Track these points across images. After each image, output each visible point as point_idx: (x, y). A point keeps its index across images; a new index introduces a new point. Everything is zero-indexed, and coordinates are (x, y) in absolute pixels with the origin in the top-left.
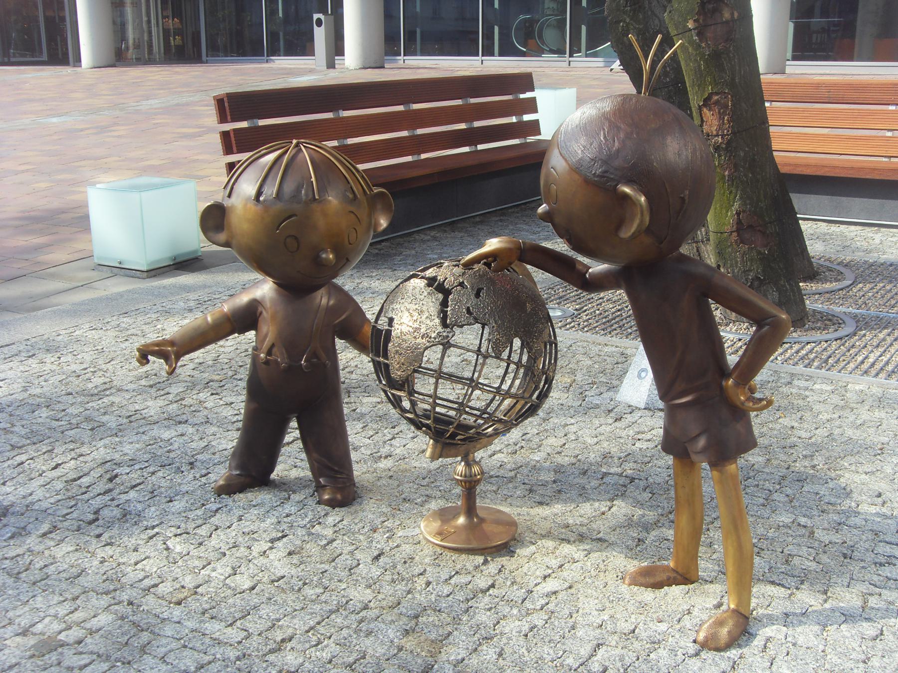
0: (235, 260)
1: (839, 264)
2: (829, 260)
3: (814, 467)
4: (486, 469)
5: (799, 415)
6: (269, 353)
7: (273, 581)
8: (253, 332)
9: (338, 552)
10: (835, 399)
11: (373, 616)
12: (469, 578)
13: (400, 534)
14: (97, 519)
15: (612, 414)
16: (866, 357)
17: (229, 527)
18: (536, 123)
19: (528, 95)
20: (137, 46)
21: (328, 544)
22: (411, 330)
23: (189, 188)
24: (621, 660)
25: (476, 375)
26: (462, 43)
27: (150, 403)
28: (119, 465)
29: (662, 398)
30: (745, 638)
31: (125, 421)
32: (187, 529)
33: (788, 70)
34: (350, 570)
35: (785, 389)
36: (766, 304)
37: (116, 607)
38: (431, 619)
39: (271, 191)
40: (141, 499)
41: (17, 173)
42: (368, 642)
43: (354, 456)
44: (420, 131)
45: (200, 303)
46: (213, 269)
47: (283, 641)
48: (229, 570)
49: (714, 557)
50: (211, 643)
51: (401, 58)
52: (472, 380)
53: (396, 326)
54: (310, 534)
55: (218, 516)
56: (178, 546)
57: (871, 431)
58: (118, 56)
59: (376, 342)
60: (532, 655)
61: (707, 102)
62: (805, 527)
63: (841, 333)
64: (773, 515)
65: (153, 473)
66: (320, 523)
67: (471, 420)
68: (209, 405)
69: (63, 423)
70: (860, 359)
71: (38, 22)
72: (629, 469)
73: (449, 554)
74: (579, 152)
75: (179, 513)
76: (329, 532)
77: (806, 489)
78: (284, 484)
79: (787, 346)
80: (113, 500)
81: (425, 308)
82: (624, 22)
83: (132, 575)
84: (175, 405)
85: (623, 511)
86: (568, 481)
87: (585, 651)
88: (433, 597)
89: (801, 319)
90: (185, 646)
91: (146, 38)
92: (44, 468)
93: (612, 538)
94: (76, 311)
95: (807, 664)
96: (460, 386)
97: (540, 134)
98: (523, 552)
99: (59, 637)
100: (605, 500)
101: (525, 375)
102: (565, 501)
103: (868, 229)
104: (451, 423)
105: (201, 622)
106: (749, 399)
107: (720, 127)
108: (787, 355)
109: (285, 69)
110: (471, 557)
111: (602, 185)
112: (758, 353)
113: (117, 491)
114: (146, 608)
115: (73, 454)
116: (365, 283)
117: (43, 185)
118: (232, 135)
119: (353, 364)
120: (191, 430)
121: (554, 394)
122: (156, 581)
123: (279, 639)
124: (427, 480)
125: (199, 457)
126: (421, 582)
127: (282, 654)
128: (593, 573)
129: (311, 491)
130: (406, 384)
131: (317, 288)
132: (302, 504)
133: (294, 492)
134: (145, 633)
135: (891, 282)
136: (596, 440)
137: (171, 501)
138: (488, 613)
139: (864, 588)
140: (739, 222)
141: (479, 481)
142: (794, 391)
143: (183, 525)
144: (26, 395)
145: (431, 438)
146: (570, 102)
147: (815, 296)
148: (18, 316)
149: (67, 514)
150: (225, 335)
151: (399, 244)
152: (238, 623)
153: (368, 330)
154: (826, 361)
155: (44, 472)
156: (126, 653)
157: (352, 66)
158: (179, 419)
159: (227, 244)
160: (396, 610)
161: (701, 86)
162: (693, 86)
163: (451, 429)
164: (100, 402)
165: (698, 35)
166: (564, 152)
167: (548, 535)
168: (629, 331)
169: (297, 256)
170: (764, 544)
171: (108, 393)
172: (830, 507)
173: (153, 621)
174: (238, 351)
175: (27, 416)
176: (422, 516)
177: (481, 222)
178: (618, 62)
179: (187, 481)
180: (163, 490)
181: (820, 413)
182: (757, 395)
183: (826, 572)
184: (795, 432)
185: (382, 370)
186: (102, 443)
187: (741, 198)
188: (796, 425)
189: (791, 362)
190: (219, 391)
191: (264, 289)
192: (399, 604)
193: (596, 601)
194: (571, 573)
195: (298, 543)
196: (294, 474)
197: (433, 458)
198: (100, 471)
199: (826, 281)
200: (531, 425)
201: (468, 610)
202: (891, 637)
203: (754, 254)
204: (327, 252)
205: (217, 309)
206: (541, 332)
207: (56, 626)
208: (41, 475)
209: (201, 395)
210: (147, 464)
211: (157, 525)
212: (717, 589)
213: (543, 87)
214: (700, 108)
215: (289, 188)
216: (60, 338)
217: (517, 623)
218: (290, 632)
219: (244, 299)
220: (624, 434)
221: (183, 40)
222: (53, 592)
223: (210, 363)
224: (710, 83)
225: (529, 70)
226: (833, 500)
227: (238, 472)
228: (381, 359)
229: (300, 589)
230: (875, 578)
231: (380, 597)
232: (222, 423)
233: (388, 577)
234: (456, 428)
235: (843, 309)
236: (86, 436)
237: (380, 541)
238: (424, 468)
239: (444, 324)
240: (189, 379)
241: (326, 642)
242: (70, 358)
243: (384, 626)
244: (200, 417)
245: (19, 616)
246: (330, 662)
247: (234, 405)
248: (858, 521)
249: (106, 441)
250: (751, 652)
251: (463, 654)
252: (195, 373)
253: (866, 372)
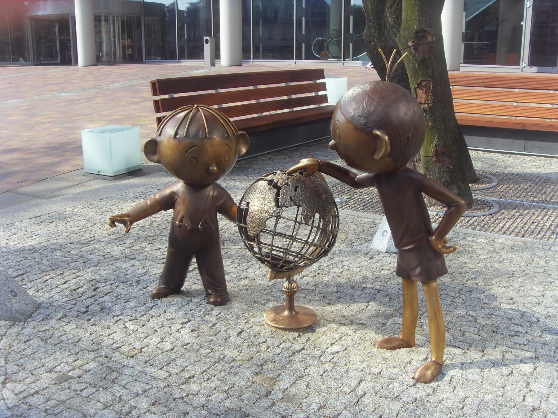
0: (160, 170)
1: (490, 174)
2: (484, 172)
3: (477, 284)
4: (299, 285)
5: (469, 256)
6: (181, 221)
7: (183, 346)
8: (172, 210)
9: (219, 330)
10: (488, 247)
11: (238, 365)
12: (290, 344)
13: (252, 320)
14: (88, 311)
15: (368, 255)
16: (505, 225)
17: (159, 316)
18: (325, 96)
19: (321, 81)
20: (108, 55)
21: (213, 326)
22: (259, 209)
23: (136, 131)
24: (373, 389)
25: (295, 233)
26: (284, 52)
27: (115, 248)
28: (98, 282)
29: (396, 246)
30: (440, 376)
31: (102, 258)
33: (461, 69)
34: (225, 340)
35: (461, 242)
36: (452, 195)
37: (99, 359)
38: (270, 367)
39: (182, 132)
41: (43, 123)
42: (236, 379)
43: (227, 278)
44: (262, 100)
45: (142, 194)
46: (149, 175)
47: (189, 378)
48: (159, 340)
49: (424, 333)
50: (150, 378)
51: (251, 60)
52: (292, 236)
53: (251, 207)
54: (203, 320)
55: (153, 310)
56: (131, 326)
57: (508, 264)
58: (98, 59)
59: (240, 216)
60: (325, 386)
61: (419, 86)
62: (472, 316)
63: (491, 211)
64: (455, 310)
65: (117, 286)
66: (208, 314)
67: (291, 258)
68: (147, 249)
69: (68, 259)
70: (501, 225)
71: (56, 42)
72: (377, 285)
73: (279, 331)
74: (352, 112)
76: (213, 319)
77: (473, 296)
79: (462, 218)
80: (96, 301)
81: (267, 197)
82: (374, 42)
83: (107, 341)
84: (129, 250)
85: (374, 308)
86: (344, 292)
87: (354, 384)
88: (271, 355)
89: (470, 204)
90: (136, 380)
91: (113, 50)
92: (59, 283)
93: (368, 323)
94: (75, 198)
95: (473, 389)
96: (285, 239)
97: (327, 102)
98: (320, 330)
99: (69, 374)
100: (364, 302)
101: (321, 234)
102: (343, 303)
103: (505, 155)
104: (281, 260)
105: (144, 367)
106: (443, 247)
107: (426, 99)
108: (463, 223)
109: (188, 66)
110: (292, 333)
111: (364, 129)
112: (448, 222)
113: (98, 296)
114: (115, 359)
115: (74, 276)
116: (232, 183)
117: (57, 130)
118: (160, 102)
119: (226, 227)
120: (137, 263)
121: (336, 244)
122: (120, 345)
123: (187, 377)
124: (267, 291)
126: (264, 346)
127: (189, 385)
128: (358, 342)
130: (255, 238)
131: (208, 185)
132: (199, 304)
133: (194, 297)
134: (115, 373)
135: (517, 184)
136: (359, 269)
137: (127, 302)
138: (301, 363)
139: (503, 348)
140: (437, 151)
141: (295, 292)
142: (466, 243)
143: (134, 315)
144: (49, 243)
146: (345, 85)
147: (477, 192)
148: (44, 201)
149: (72, 308)
150: (156, 212)
152: (165, 368)
153: (235, 209)
154: (483, 227)
155: (59, 285)
156: (104, 383)
157: (225, 64)
158: (131, 257)
159: (158, 162)
160: (250, 362)
161: (416, 76)
162: (411, 77)
163: (281, 263)
164: (88, 248)
165: (414, 49)
166: (343, 112)
167: (333, 321)
168: (377, 210)
169: (197, 167)
170: (451, 326)
171: (92, 243)
172: (486, 305)
173: (119, 366)
174: (163, 220)
175: (49, 255)
176: (265, 311)
177: (296, 150)
178: (370, 63)
179: (136, 291)
180: (123, 295)
181: (480, 255)
182: (448, 245)
183: (483, 340)
184: (467, 265)
185: (243, 231)
186: (89, 270)
187: (438, 138)
188: (467, 261)
189: (465, 227)
190: (153, 242)
191: (179, 186)
192: (252, 358)
193: (360, 357)
194: (346, 342)
195: (197, 325)
196: (194, 287)
197: (271, 279)
198: (89, 285)
199: (483, 183)
200: (324, 261)
201: (290, 362)
202: (517, 374)
203: (445, 168)
204: (213, 166)
205: (152, 197)
206: (330, 210)
207: (67, 368)
208: (57, 287)
210: (114, 282)
212: (425, 350)
213: (330, 76)
214: (415, 89)
215: (193, 131)
216: (67, 212)
217: (317, 369)
218: (193, 373)
219: (168, 191)
220: (374, 266)
221: (132, 51)
222: (65, 350)
223: (148, 226)
224: (421, 75)
225: (321, 67)
226: (487, 302)
229: (198, 350)
230: (509, 343)
231: (242, 354)
232: (154, 259)
233: (246, 344)
235: (492, 198)
236: (81, 266)
237: (241, 324)
239: (278, 206)
240: (136, 235)
241: (212, 379)
242: (72, 223)
243: (244, 370)
244: (142, 256)
245: (48, 362)
246: (215, 389)
247: (161, 250)
248: (500, 313)
249: (92, 269)
250: (443, 383)
251: (287, 385)
252: (140, 232)
253: (504, 233)
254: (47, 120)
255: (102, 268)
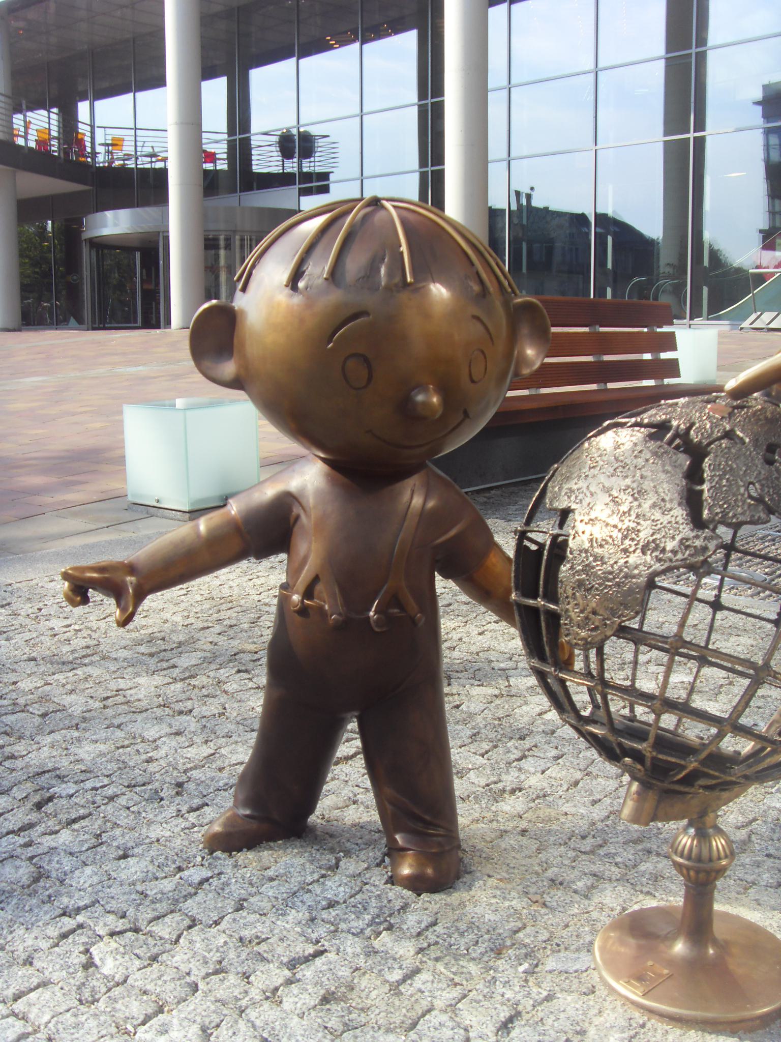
6: (308, 593)
8: (283, 556)
9: (425, 1004)
17: (216, 923)
18: (674, 363)
19: (666, 329)
21: (404, 980)
31: (98, 705)
32: (136, 920)
39: (318, 270)
40: (76, 849)
41: (74, 414)
43: (460, 787)
53: (580, 527)
54: (371, 952)
55: (200, 897)
56: (110, 960)
65: (111, 799)
66: (390, 928)
68: (231, 687)
73: (662, 1026)
75: (133, 884)
78: (332, 836)
81: (648, 485)
84: (179, 685)
97: (679, 376)
113: (40, 829)
117: (98, 425)
119: (455, 636)
125: (195, 774)
129: (379, 854)
133: (348, 853)
137: (125, 856)
143: (131, 912)
145: (634, 778)
151: (512, 493)
163: (692, 764)
164: (71, 674)
171: (86, 661)
186: (49, 739)
190: (250, 666)
191: (309, 477)
195: (344, 972)
196: (352, 815)
198: (29, 787)
204: (425, 390)
209: (222, 671)
210: (106, 781)
211: (86, 907)
215: (354, 265)
219: (269, 492)
223: (246, 626)
227: (248, 812)
228: (540, 602)
234: (703, 763)
238: (583, 817)
239: (697, 522)
254: (83, 409)
255: (87, 735)
